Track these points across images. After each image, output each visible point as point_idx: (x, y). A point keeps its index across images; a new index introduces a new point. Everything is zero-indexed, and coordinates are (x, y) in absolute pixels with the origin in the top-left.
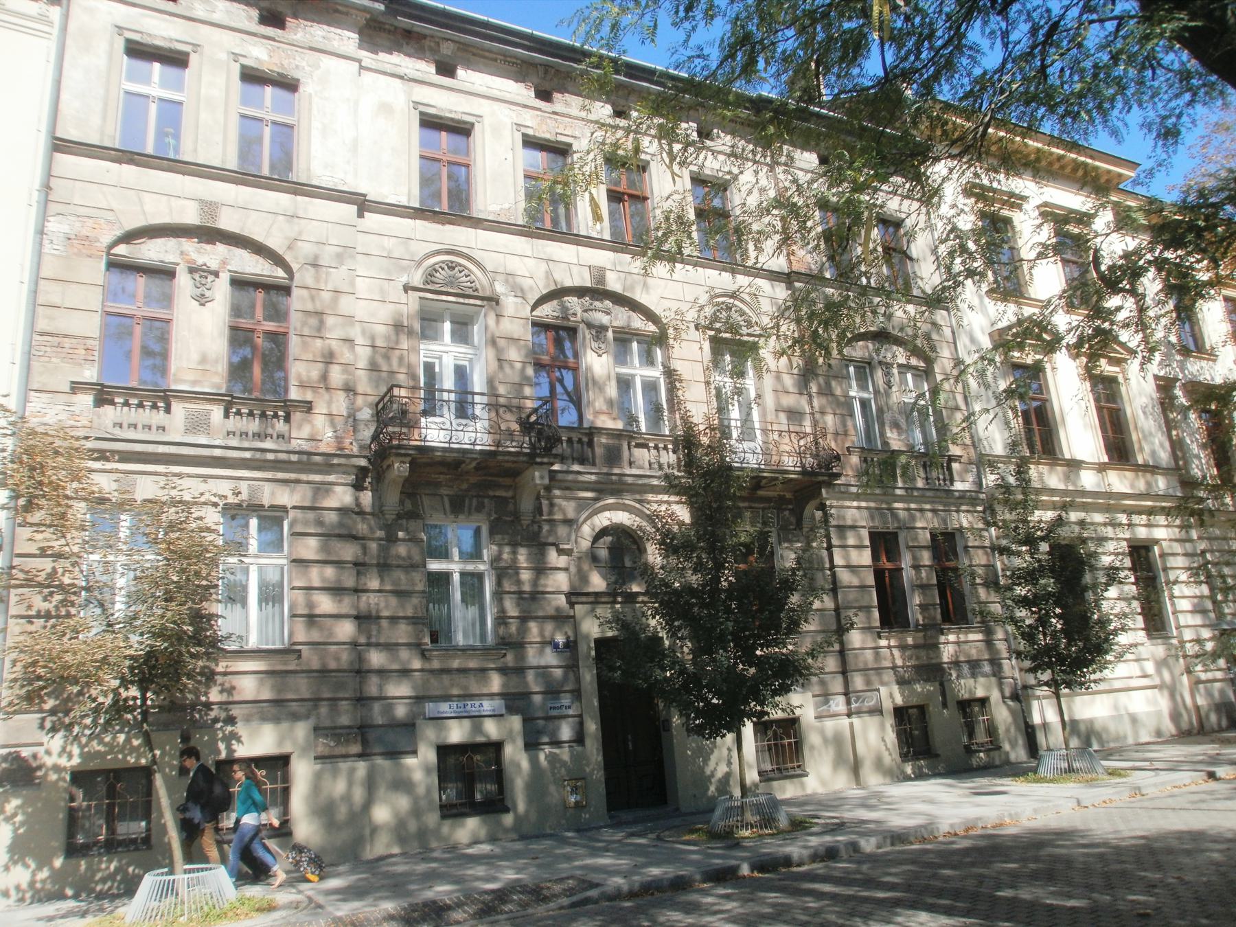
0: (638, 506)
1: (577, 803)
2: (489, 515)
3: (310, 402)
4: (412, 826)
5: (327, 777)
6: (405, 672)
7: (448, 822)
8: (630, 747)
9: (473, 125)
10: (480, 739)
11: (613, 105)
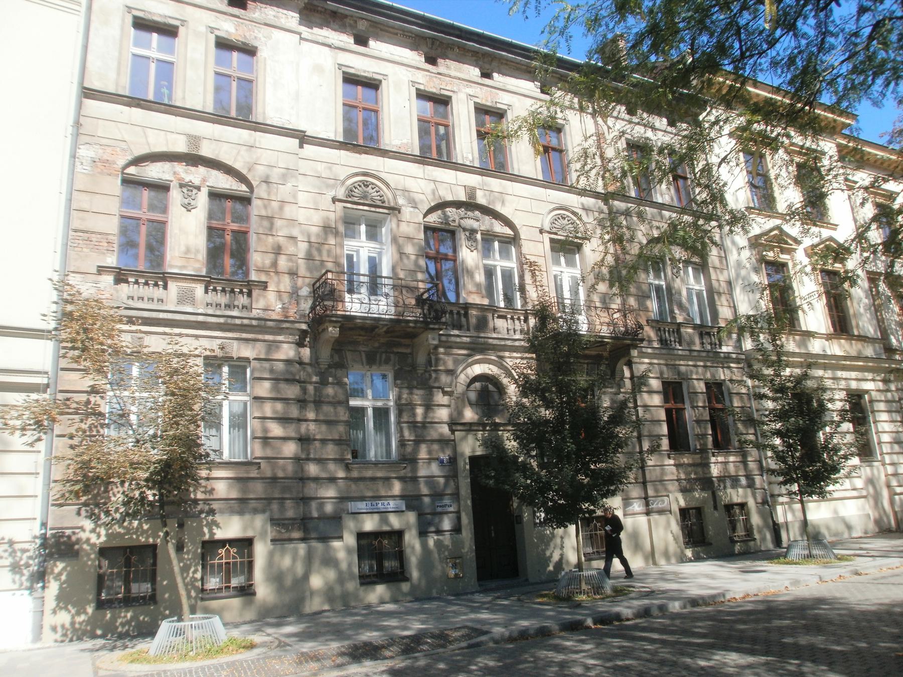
1: (456, 575)
2: (394, 365)
3: (266, 283)
4: (338, 590)
6: (333, 480)
7: (363, 588)
10: (386, 528)
11: (481, 69)
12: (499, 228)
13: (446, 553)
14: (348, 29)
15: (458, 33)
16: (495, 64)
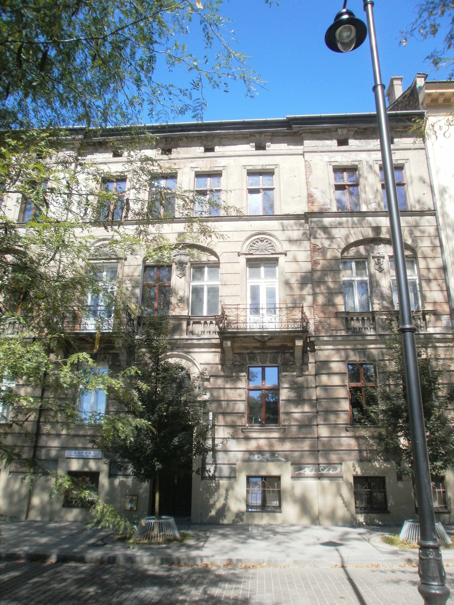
0: (185, 355)
1: (131, 508)
2: (108, 362)
4: (48, 509)
5: (12, 481)
6: (58, 435)
7: (65, 509)
8: (176, 482)
9: (222, 171)
10: (86, 470)
11: (205, 146)
12: (205, 257)
13: (127, 491)
14: (109, 149)
15: (180, 129)
16: (216, 140)
